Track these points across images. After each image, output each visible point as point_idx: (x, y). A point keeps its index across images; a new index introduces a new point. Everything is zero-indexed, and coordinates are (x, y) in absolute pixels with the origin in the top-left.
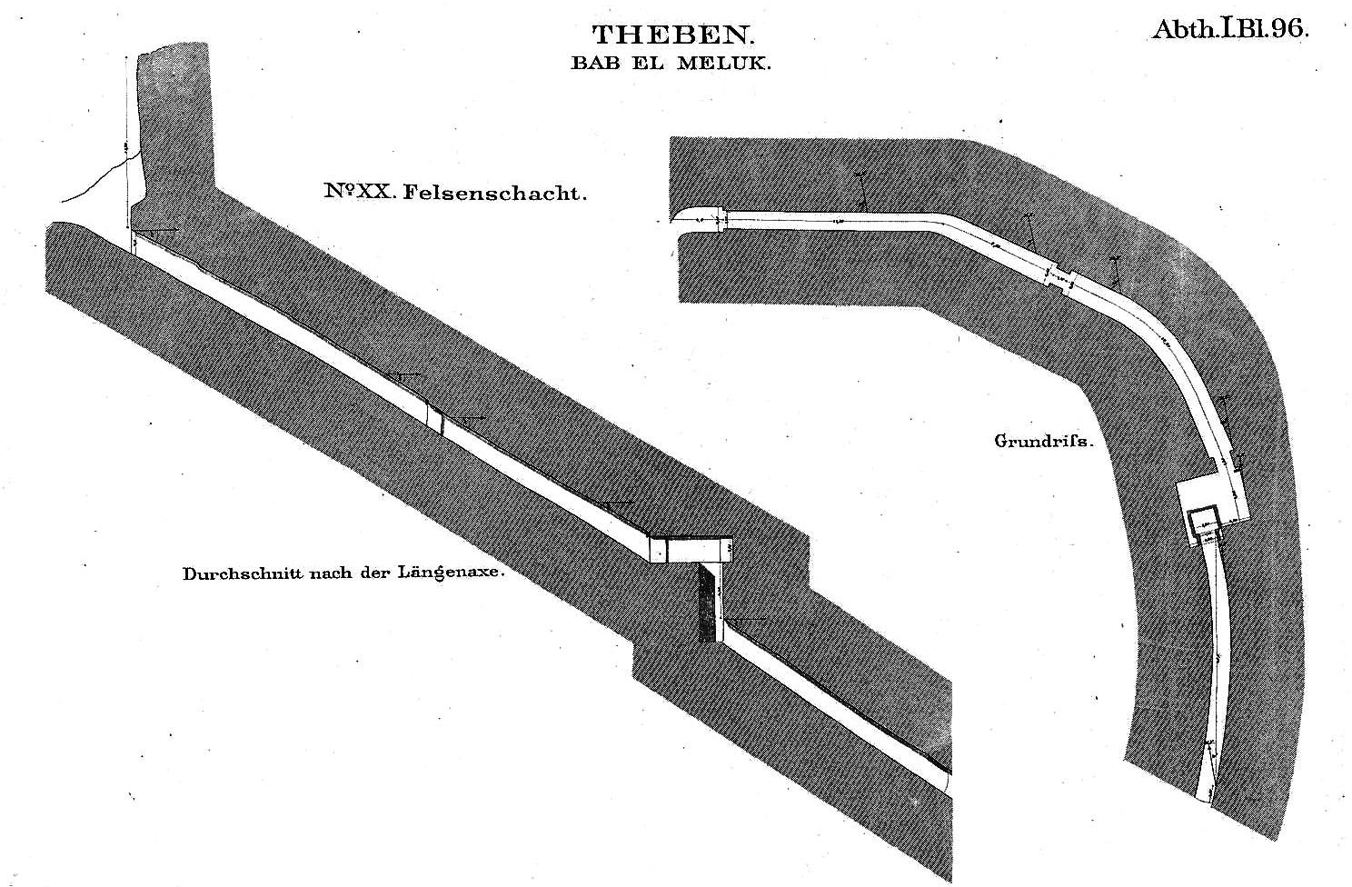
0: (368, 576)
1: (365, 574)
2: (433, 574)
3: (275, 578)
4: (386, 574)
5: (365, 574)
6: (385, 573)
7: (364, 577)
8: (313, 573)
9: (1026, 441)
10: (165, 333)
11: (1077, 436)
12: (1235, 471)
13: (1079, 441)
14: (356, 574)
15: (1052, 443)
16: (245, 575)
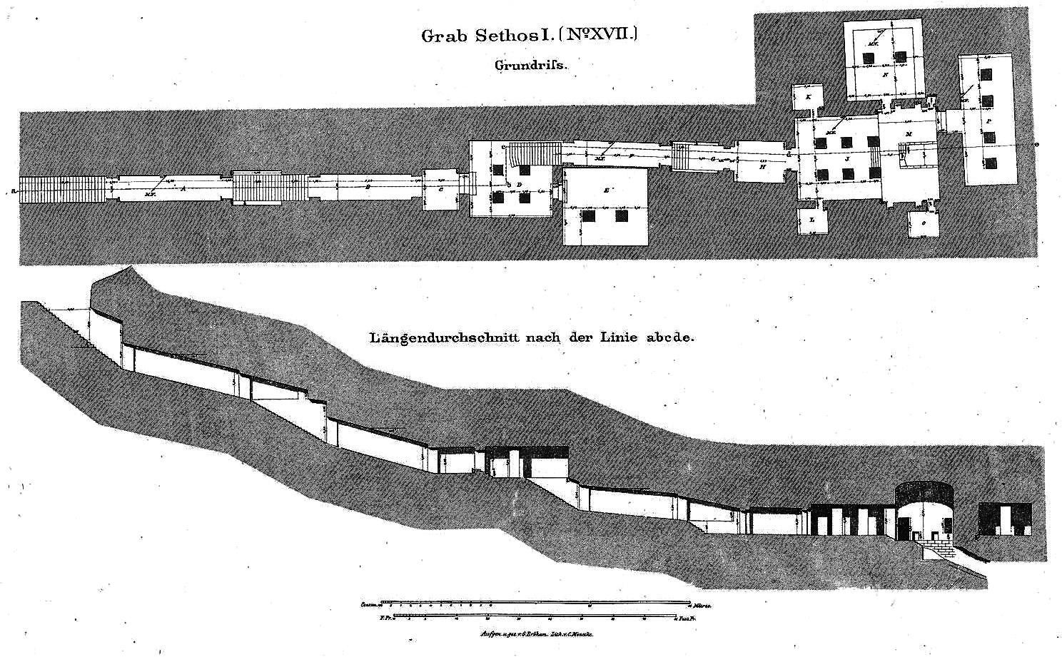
0: (576, 341)
1: (573, 339)
2: (400, 341)
3: (618, 340)
4: (590, 339)
5: (573, 339)
6: (588, 338)
7: (572, 341)
8: (528, 337)
9: (518, 65)
10: (995, 458)
11: (556, 61)
12: (660, 164)
13: (558, 65)
14: (522, 338)
15: (538, 66)
16: (472, 339)
